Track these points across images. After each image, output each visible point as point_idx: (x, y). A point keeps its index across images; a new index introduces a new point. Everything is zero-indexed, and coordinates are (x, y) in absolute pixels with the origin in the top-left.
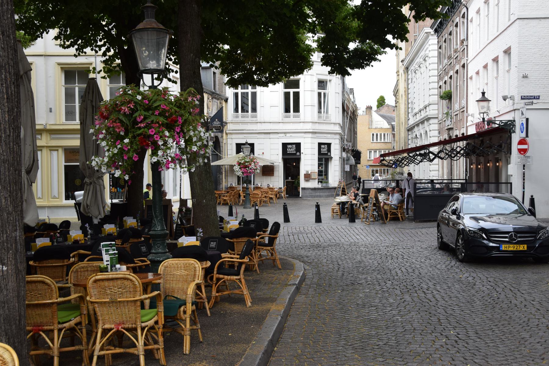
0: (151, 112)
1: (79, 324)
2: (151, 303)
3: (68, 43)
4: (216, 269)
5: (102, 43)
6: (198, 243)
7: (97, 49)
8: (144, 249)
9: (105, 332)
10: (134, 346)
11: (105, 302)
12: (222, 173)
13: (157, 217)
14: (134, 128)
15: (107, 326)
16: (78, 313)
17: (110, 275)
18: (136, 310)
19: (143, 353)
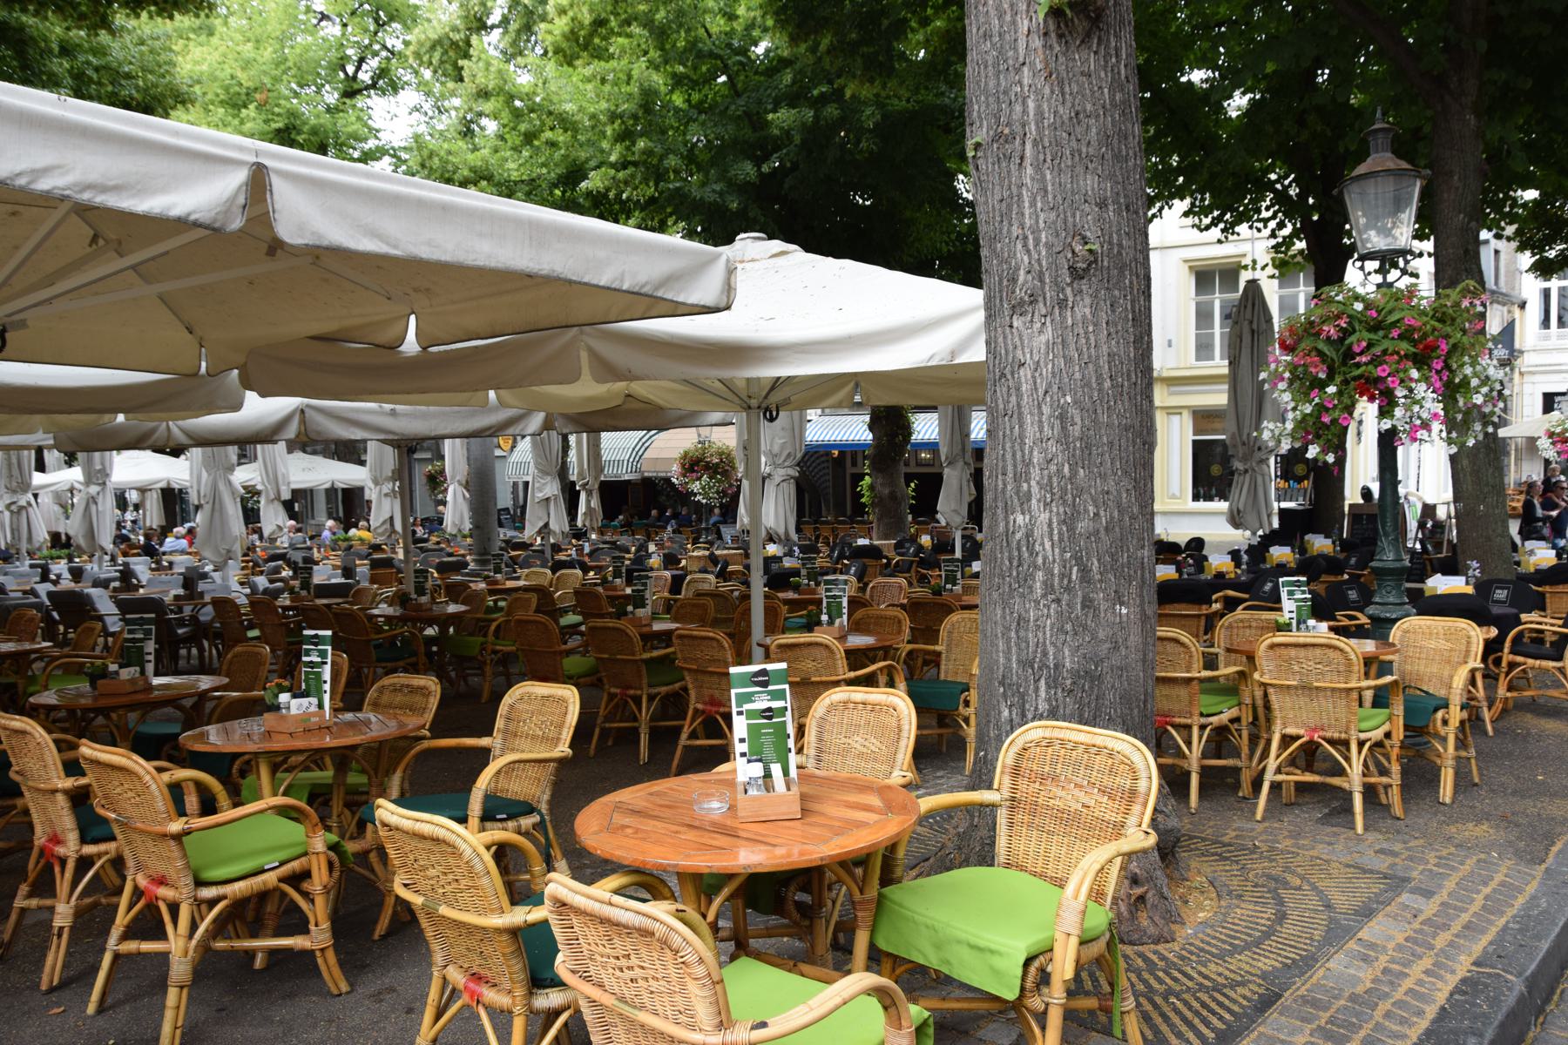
0: (1381, 333)
1: (1236, 720)
2: (1375, 696)
3: (1206, 221)
4: (1507, 644)
5: (1270, 214)
6: (1470, 590)
7: (1260, 225)
8: (1353, 595)
9: (1287, 740)
10: (1341, 772)
11: (1289, 687)
12: (1508, 454)
13: (1386, 535)
14: (1344, 363)
15: (1291, 731)
16: (1235, 702)
17: (1294, 637)
18: (1348, 706)
19: (1360, 789)
